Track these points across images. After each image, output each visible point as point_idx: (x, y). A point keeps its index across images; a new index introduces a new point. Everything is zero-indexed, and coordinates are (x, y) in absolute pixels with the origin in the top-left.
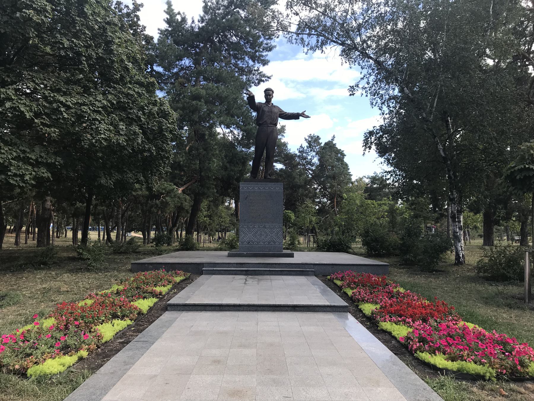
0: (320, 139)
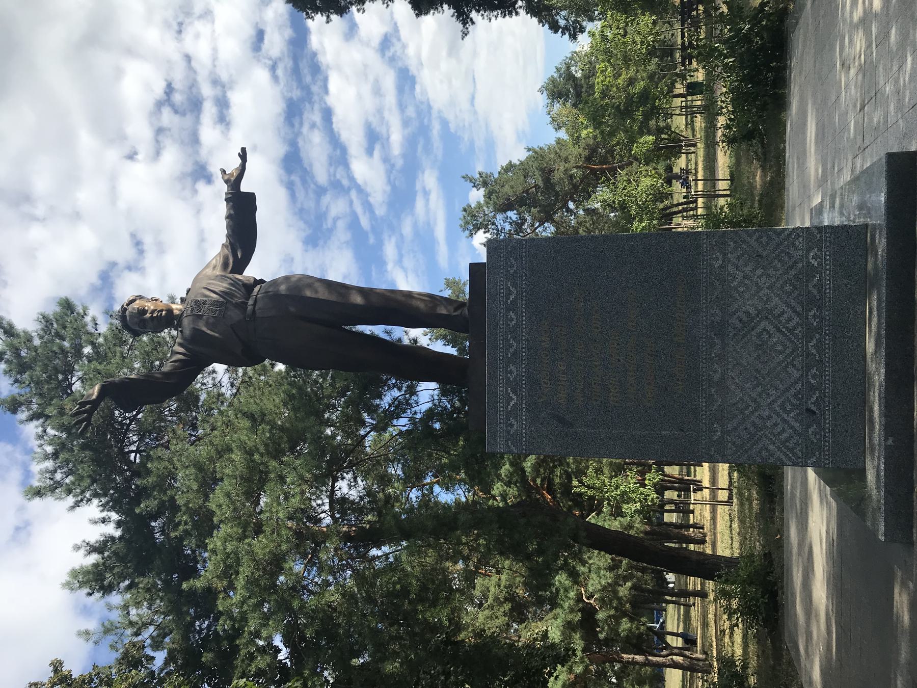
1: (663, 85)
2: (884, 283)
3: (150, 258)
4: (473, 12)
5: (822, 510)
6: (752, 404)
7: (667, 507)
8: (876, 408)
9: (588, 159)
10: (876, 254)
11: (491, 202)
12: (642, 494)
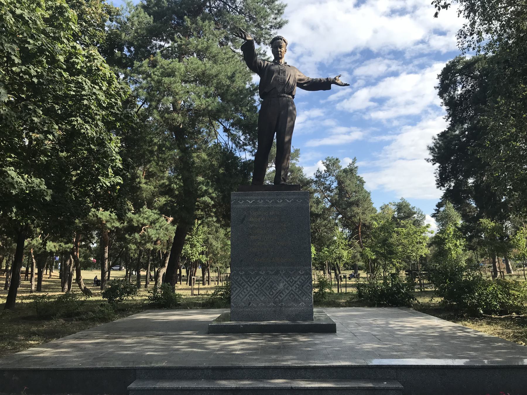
0: (339, 162)
9: (364, 225)
11: (341, 174)
12: (196, 253)
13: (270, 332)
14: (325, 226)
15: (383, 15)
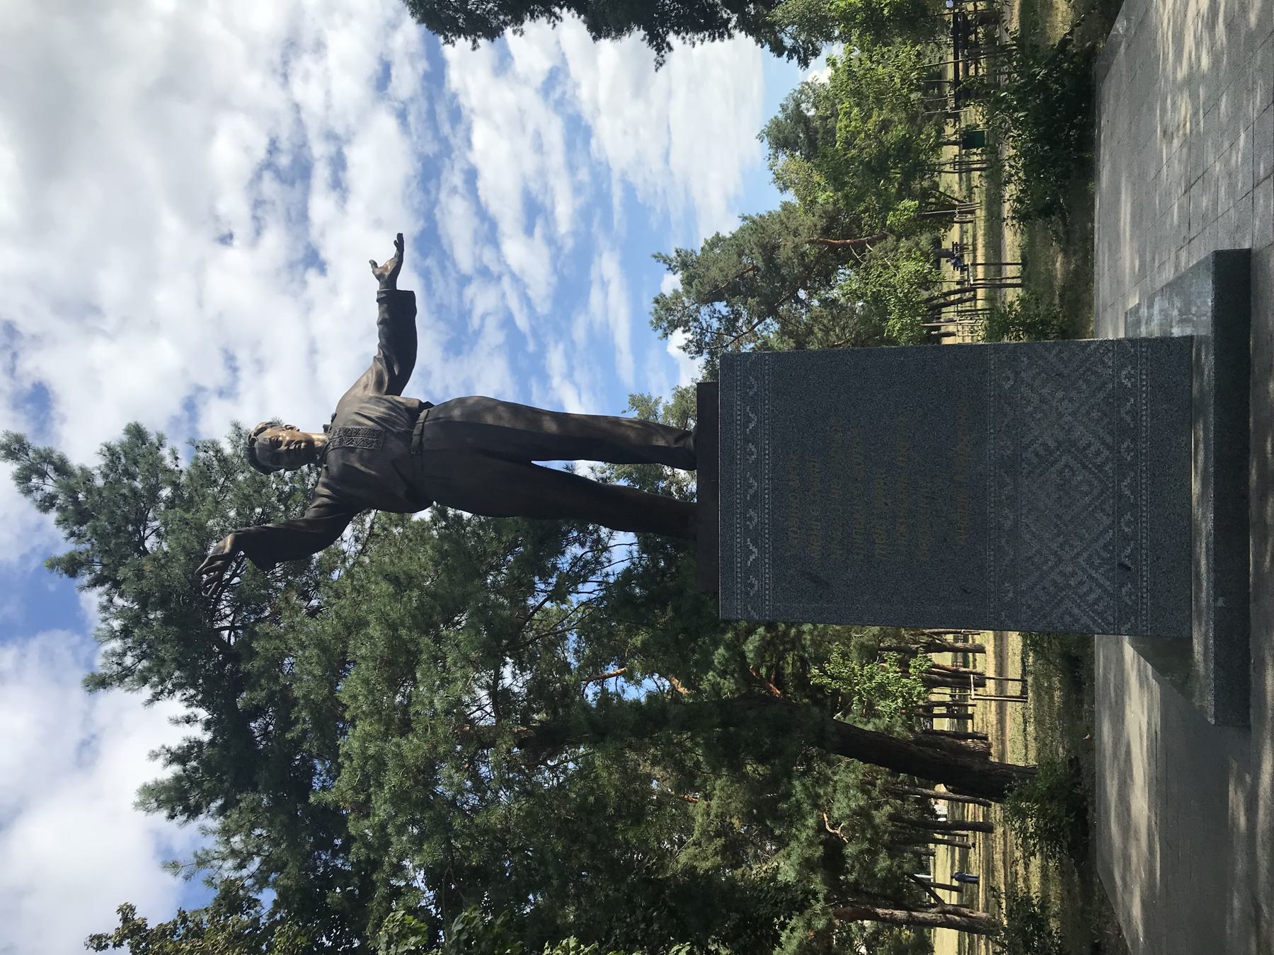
1: (930, 130)
2: (1211, 409)
3: (246, 374)
4: (671, 34)
5: (1141, 698)
6: (1052, 557)
7: (936, 711)
8: (1203, 562)
9: (826, 231)
10: (1203, 374)
11: (694, 290)
12: (905, 686)
13: (1245, 497)
14: (827, 331)
15: (342, 207)
